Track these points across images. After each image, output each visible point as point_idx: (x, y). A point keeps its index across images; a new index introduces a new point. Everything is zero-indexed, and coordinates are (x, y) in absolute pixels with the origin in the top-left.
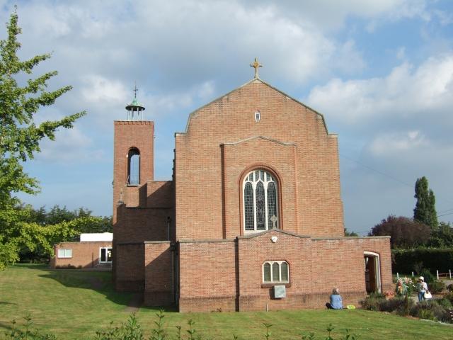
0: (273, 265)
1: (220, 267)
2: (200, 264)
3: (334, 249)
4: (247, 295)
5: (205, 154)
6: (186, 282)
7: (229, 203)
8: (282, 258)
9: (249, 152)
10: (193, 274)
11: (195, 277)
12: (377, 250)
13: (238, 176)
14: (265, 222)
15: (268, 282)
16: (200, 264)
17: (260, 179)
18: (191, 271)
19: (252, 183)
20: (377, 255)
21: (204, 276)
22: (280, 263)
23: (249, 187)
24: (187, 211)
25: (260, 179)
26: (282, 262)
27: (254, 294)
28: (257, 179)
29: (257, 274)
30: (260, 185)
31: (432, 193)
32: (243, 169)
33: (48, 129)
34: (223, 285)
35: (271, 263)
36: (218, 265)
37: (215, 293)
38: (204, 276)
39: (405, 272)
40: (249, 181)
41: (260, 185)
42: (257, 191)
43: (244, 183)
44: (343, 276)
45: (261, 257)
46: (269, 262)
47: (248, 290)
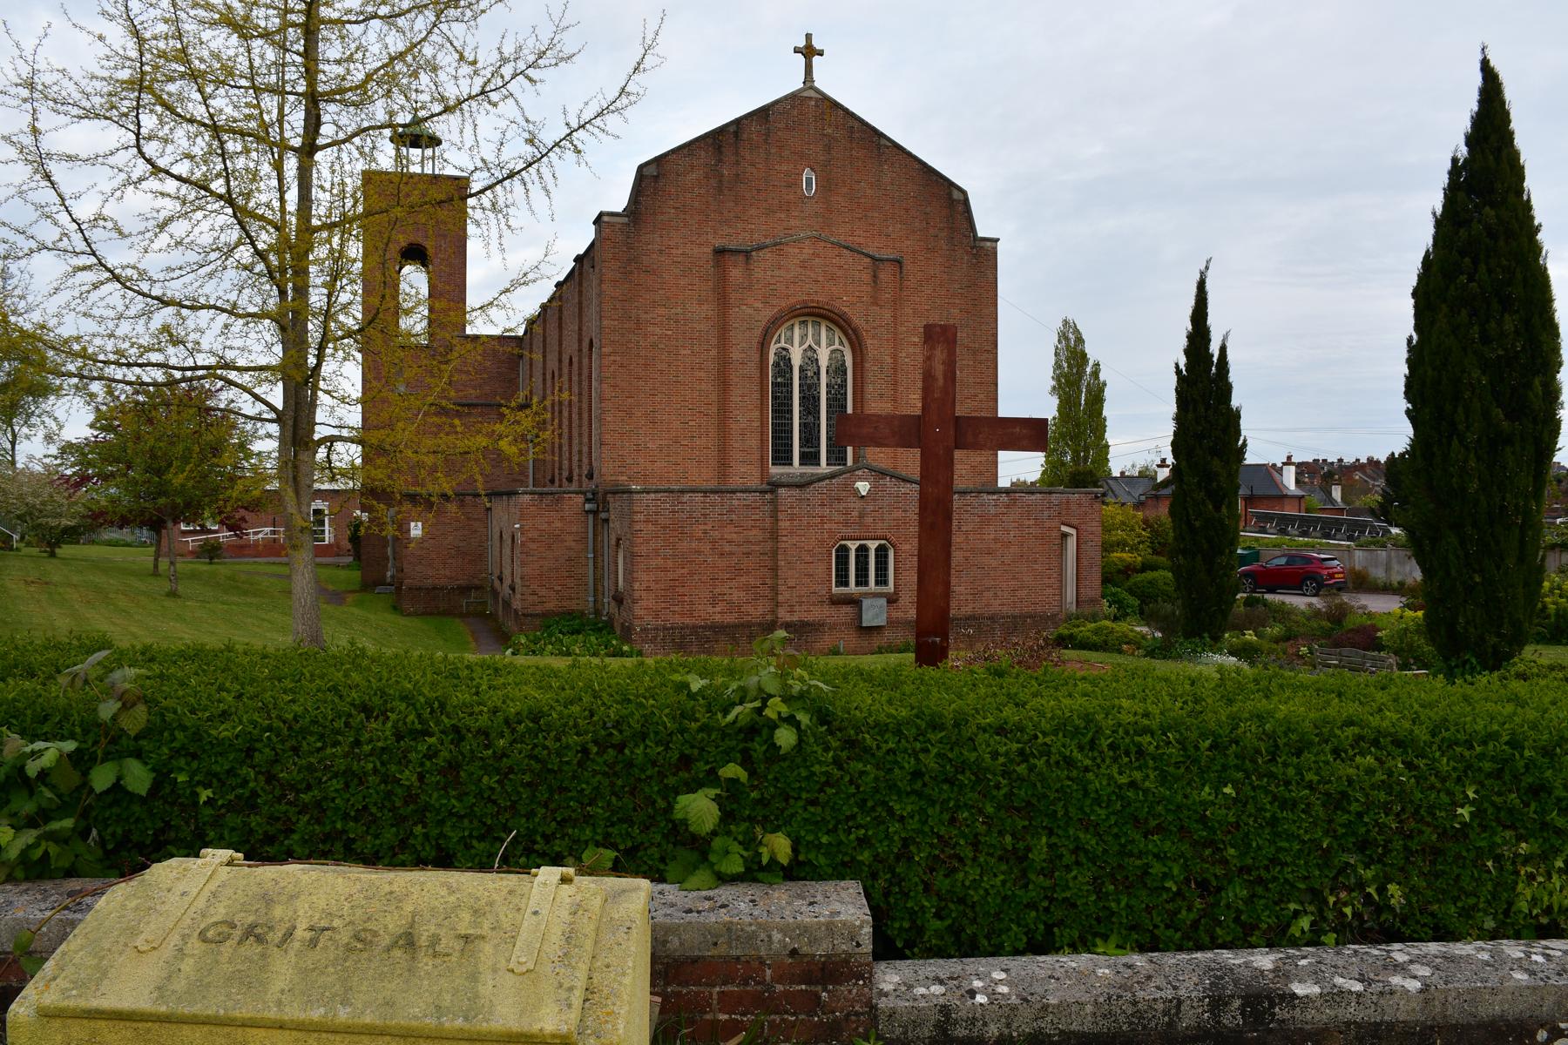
0: (877, 550)
1: (731, 553)
2: (684, 545)
3: (996, 515)
4: (795, 619)
5: (677, 271)
6: (648, 589)
7: (735, 396)
8: (879, 533)
9: (788, 270)
10: (665, 570)
11: (671, 575)
12: (1075, 522)
13: (758, 332)
14: (819, 445)
15: (883, 589)
16: (684, 545)
17: (810, 341)
18: (660, 562)
19: (791, 350)
20: (1073, 532)
21: (691, 574)
22: (873, 545)
23: (784, 362)
24: (630, 415)
25: (810, 341)
26: (877, 543)
27: (809, 618)
28: (830, 343)
29: (820, 569)
30: (811, 359)
31: (1245, 444)
32: (767, 314)
33: (1223, 349)
34: (737, 595)
35: (853, 546)
36: (727, 548)
37: (717, 614)
38: (691, 574)
39: (1224, 598)
40: (783, 344)
41: (811, 359)
42: (802, 369)
43: (773, 349)
44: (1014, 578)
45: (830, 531)
46: (849, 543)
47: (797, 608)
